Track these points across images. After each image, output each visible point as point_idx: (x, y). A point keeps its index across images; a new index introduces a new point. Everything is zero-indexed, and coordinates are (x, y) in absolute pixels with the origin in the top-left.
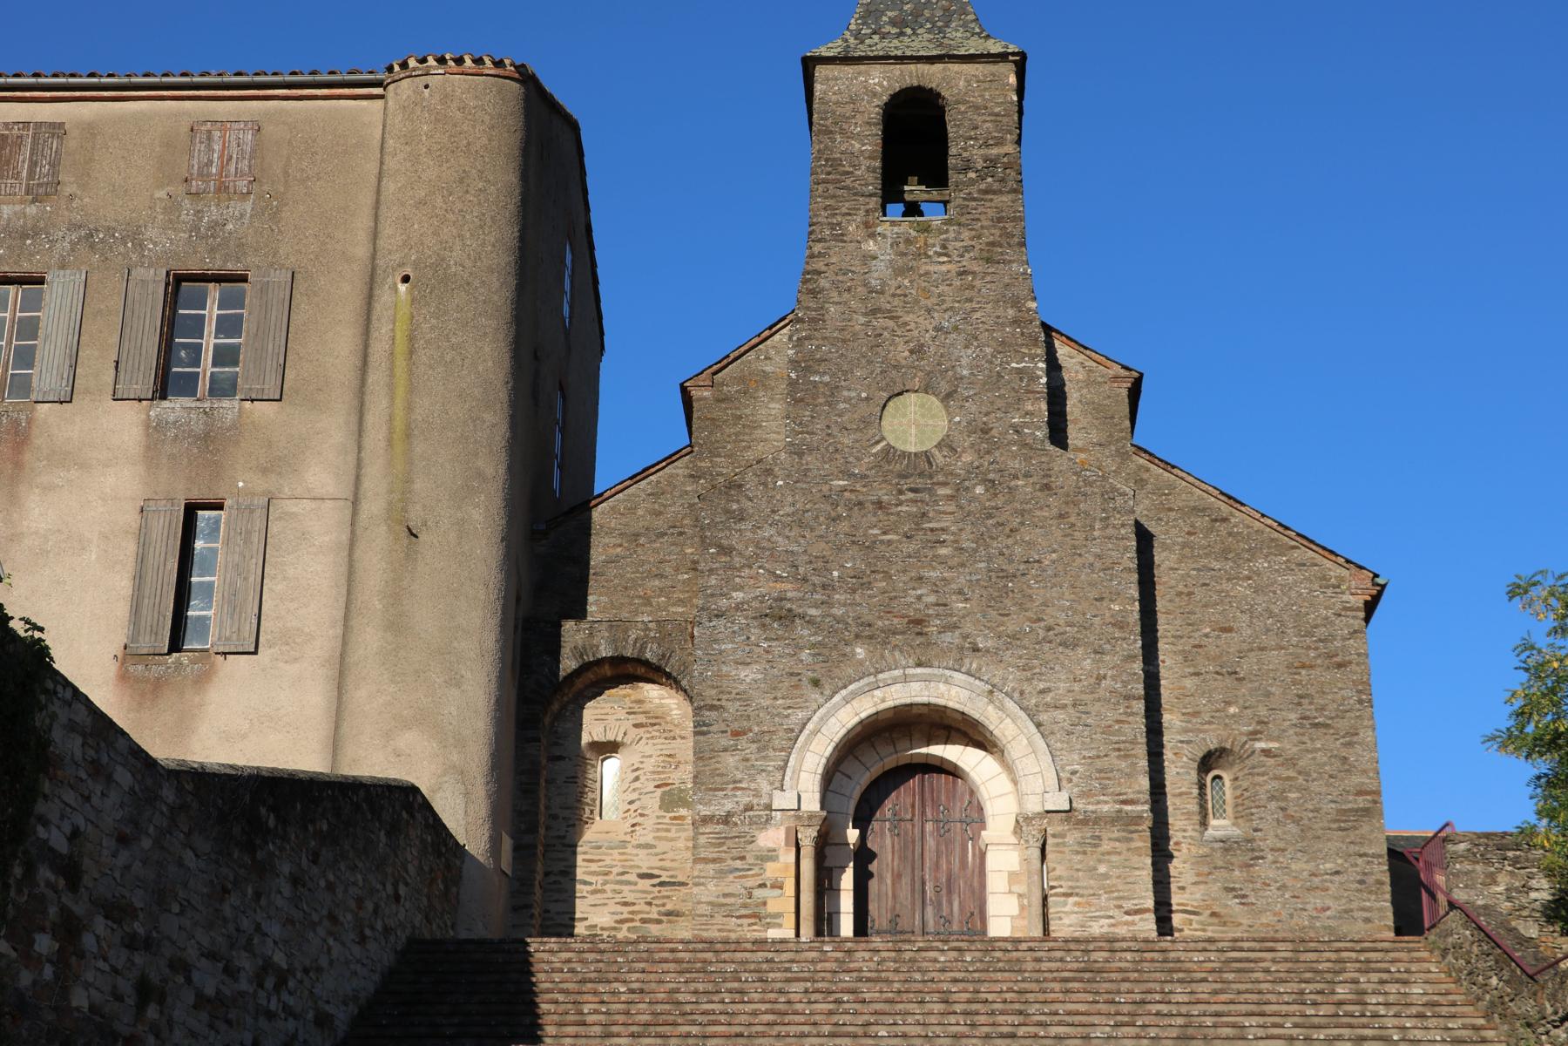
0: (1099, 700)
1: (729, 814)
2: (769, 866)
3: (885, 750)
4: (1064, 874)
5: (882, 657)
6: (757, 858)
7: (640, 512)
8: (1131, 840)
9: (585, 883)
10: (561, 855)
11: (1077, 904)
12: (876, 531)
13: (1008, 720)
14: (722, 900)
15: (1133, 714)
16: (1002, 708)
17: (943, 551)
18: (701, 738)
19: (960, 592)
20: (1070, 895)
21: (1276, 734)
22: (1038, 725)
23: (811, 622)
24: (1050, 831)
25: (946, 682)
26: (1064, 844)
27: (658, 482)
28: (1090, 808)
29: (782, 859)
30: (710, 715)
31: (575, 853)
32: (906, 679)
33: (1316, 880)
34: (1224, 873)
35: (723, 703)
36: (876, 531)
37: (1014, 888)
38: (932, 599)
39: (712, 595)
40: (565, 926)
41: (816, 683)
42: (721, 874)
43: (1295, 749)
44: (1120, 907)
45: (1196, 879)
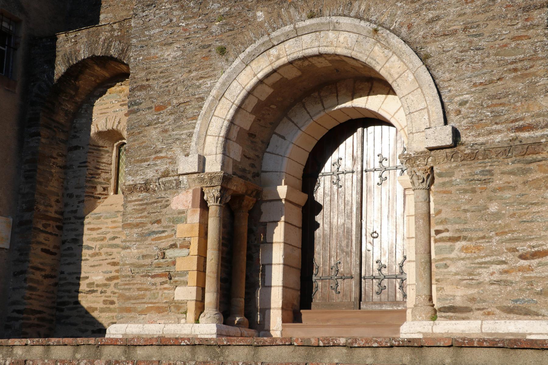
0: (493, 18)
1: (147, 183)
3: (314, 108)
5: (279, 16)
8: (529, 171)
9: (89, 248)
10: (73, 226)
11: (465, 249)
13: (395, 58)
14: (142, 262)
15: (533, 26)
16: (387, 46)
18: (133, 116)
20: (458, 239)
22: (424, 59)
24: (436, 170)
25: (335, 29)
28: (481, 140)
29: (189, 220)
30: (141, 94)
31: (82, 224)
32: (297, 34)
35: (151, 82)
40: (73, 284)
41: (222, 51)
42: (143, 236)
44: (514, 250)
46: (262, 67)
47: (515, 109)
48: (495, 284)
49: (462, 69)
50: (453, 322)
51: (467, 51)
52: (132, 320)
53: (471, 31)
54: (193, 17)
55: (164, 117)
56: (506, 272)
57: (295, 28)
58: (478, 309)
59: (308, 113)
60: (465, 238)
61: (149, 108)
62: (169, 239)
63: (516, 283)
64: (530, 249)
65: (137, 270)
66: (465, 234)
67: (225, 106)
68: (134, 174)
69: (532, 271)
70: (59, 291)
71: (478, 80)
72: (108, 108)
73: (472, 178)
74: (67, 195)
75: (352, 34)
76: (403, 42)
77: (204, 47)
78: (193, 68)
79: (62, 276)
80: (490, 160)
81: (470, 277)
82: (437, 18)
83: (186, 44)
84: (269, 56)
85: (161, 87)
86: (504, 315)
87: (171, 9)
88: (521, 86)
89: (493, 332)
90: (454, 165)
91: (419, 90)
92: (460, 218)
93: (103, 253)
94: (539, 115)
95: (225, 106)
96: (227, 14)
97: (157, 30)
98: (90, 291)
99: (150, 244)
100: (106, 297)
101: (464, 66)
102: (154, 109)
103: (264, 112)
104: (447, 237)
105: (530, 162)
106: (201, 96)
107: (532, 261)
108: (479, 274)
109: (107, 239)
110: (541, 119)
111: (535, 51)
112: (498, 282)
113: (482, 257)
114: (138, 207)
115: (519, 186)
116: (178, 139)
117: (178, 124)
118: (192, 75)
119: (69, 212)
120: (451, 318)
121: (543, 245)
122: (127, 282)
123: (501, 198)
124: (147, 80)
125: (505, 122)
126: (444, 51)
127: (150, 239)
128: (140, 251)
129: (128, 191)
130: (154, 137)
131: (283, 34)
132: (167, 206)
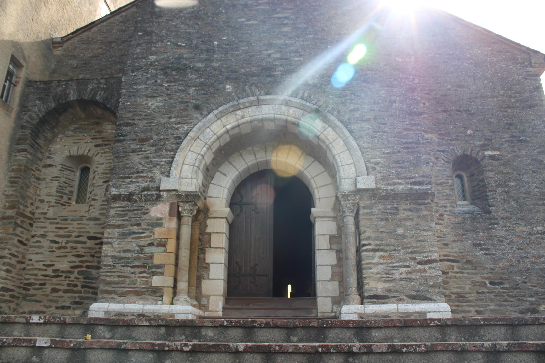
1: (131, 194)
2: (157, 230)
4: (373, 235)
5: (244, 90)
6: (148, 225)
7: (114, 31)
11: (381, 257)
12: (243, 20)
13: (330, 129)
14: (123, 255)
17: (286, 29)
19: (296, 52)
21: (497, 146)
23: (197, 70)
26: (371, 214)
27: (126, 16)
28: (390, 187)
33: (533, 238)
34: (471, 235)
35: (136, 122)
36: (243, 20)
37: (333, 247)
38: (278, 55)
39: (137, 58)
41: (197, 108)
42: (124, 235)
43: (509, 156)
44: (414, 259)
45: (455, 238)
46: (230, 122)
50: (378, 305)
51: (377, 132)
52: (113, 300)
53: (379, 120)
54: (174, 82)
55: (147, 147)
56: (410, 273)
57: (258, 99)
58: (394, 297)
60: (382, 250)
61: (133, 140)
62: (148, 239)
63: (417, 279)
65: (117, 261)
66: (382, 247)
67: (199, 145)
68: (117, 187)
70: (26, 274)
72: (80, 139)
74: (39, 200)
75: (299, 110)
77: (182, 102)
78: (173, 115)
79: (30, 262)
81: (387, 276)
82: (357, 110)
83: (167, 98)
84: (236, 115)
85: (144, 126)
86: (410, 301)
87: (157, 73)
88: (411, 158)
90: (373, 202)
91: (348, 151)
93: (69, 247)
94: (423, 176)
95: (199, 145)
96: (202, 83)
97: (144, 86)
98: (55, 276)
99: (130, 242)
100: (70, 281)
101: (376, 141)
102: (137, 140)
105: (420, 204)
106: (179, 135)
108: (393, 274)
109: (73, 236)
110: (425, 179)
111: (418, 138)
112: (405, 279)
113: (394, 263)
114: (120, 213)
116: (158, 164)
117: (159, 153)
118: (172, 120)
119: (39, 213)
120: (375, 303)
122: (109, 270)
123: (405, 225)
124: (133, 120)
127: (130, 237)
128: (121, 246)
129: (112, 199)
130: (137, 161)
131: (248, 102)
132: (147, 213)
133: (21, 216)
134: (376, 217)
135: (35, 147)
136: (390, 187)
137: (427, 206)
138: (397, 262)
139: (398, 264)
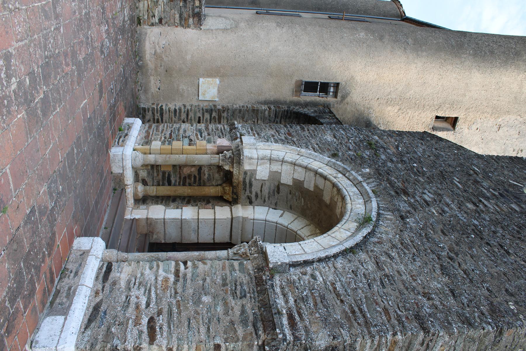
11: (166, 280)
28: (278, 290)
44: (160, 313)
47: (311, 314)
48: (127, 299)
49: (347, 274)
58: (103, 287)
59: (302, 228)
64: (158, 325)
66: (181, 280)
69: (135, 326)
71: (338, 285)
73: (238, 283)
76: (364, 235)
80: (256, 296)
86: (93, 304)
89: (77, 293)
90: (251, 272)
92: (198, 276)
94: (307, 331)
101: (351, 276)
103: (297, 194)
104: (179, 268)
105: (254, 326)
107: (146, 327)
110: (303, 332)
115: (229, 317)
121: (162, 335)
123: (216, 305)
125: (297, 306)
126: (362, 263)
133: (218, 115)
134: (228, 274)
135: (277, 119)
136: (278, 290)
137: (254, 335)
138: (157, 295)
139: (153, 295)
